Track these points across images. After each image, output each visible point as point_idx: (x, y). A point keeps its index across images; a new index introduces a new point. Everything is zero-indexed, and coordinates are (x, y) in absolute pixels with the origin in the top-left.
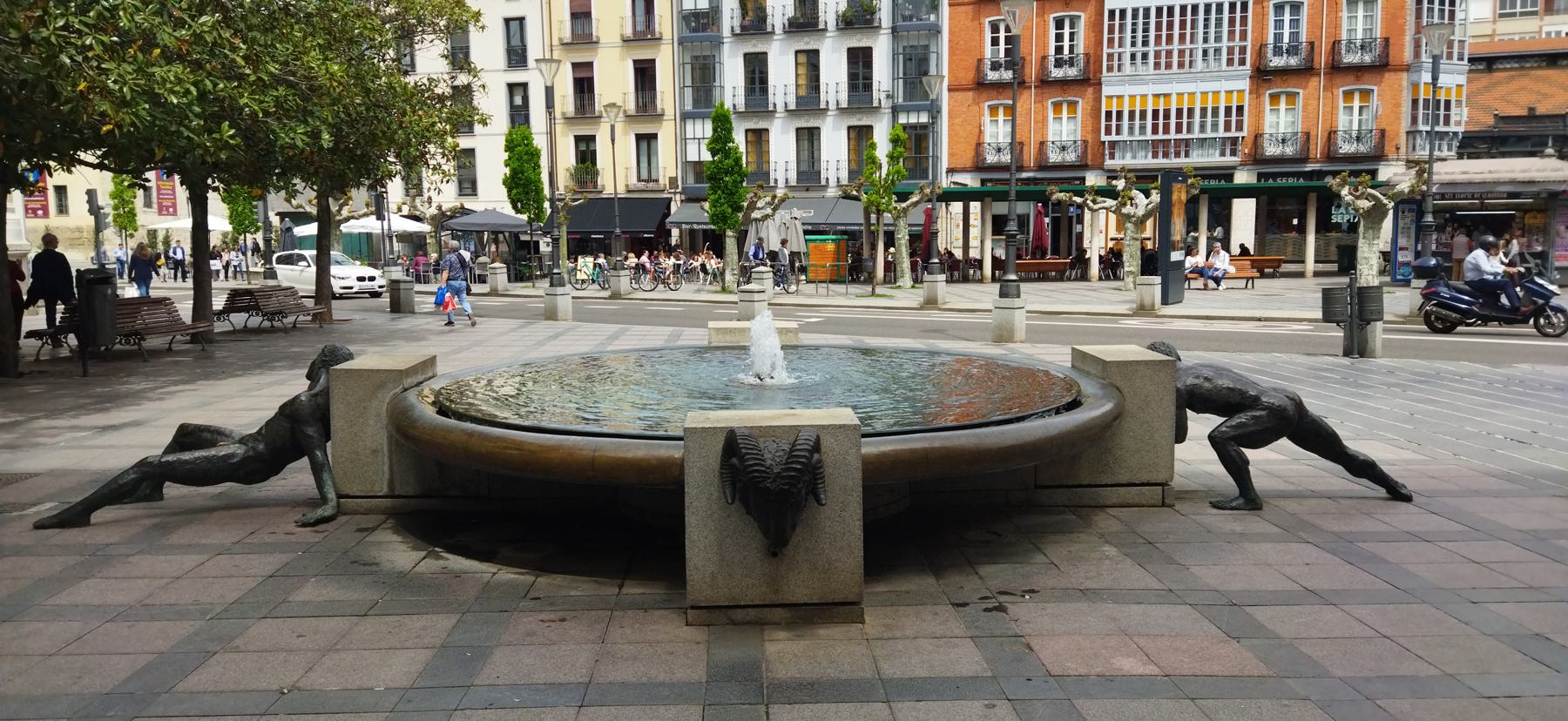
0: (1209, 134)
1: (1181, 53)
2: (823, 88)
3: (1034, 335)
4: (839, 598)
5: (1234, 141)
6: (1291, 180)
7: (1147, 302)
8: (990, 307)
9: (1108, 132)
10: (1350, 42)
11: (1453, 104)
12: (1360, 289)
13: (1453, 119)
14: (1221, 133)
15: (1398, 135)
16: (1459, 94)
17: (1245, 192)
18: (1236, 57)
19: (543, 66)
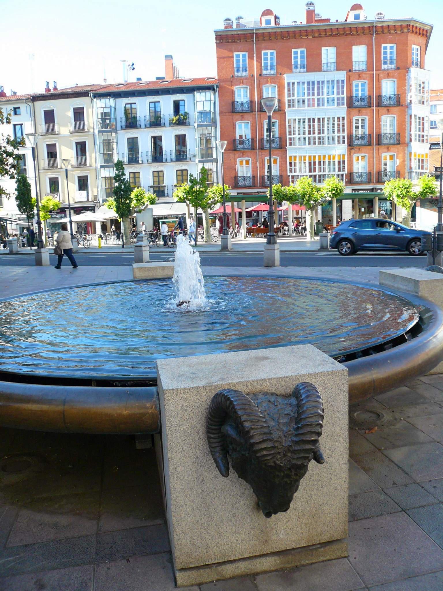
0: (333, 173)
1: (319, 138)
2: (164, 153)
3: (285, 262)
4: (325, 538)
5: (342, 175)
6: (364, 192)
7: (325, 245)
8: (263, 249)
9: (291, 171)
10: (356, 136)
11: (425, 161)
12: (78, 165)
13: (425, 167)
14: (337, 172)
15: (405, 174)
16: (427, 157)
17: (347, 197)
18: (312, 141)
19: (64, 162)
